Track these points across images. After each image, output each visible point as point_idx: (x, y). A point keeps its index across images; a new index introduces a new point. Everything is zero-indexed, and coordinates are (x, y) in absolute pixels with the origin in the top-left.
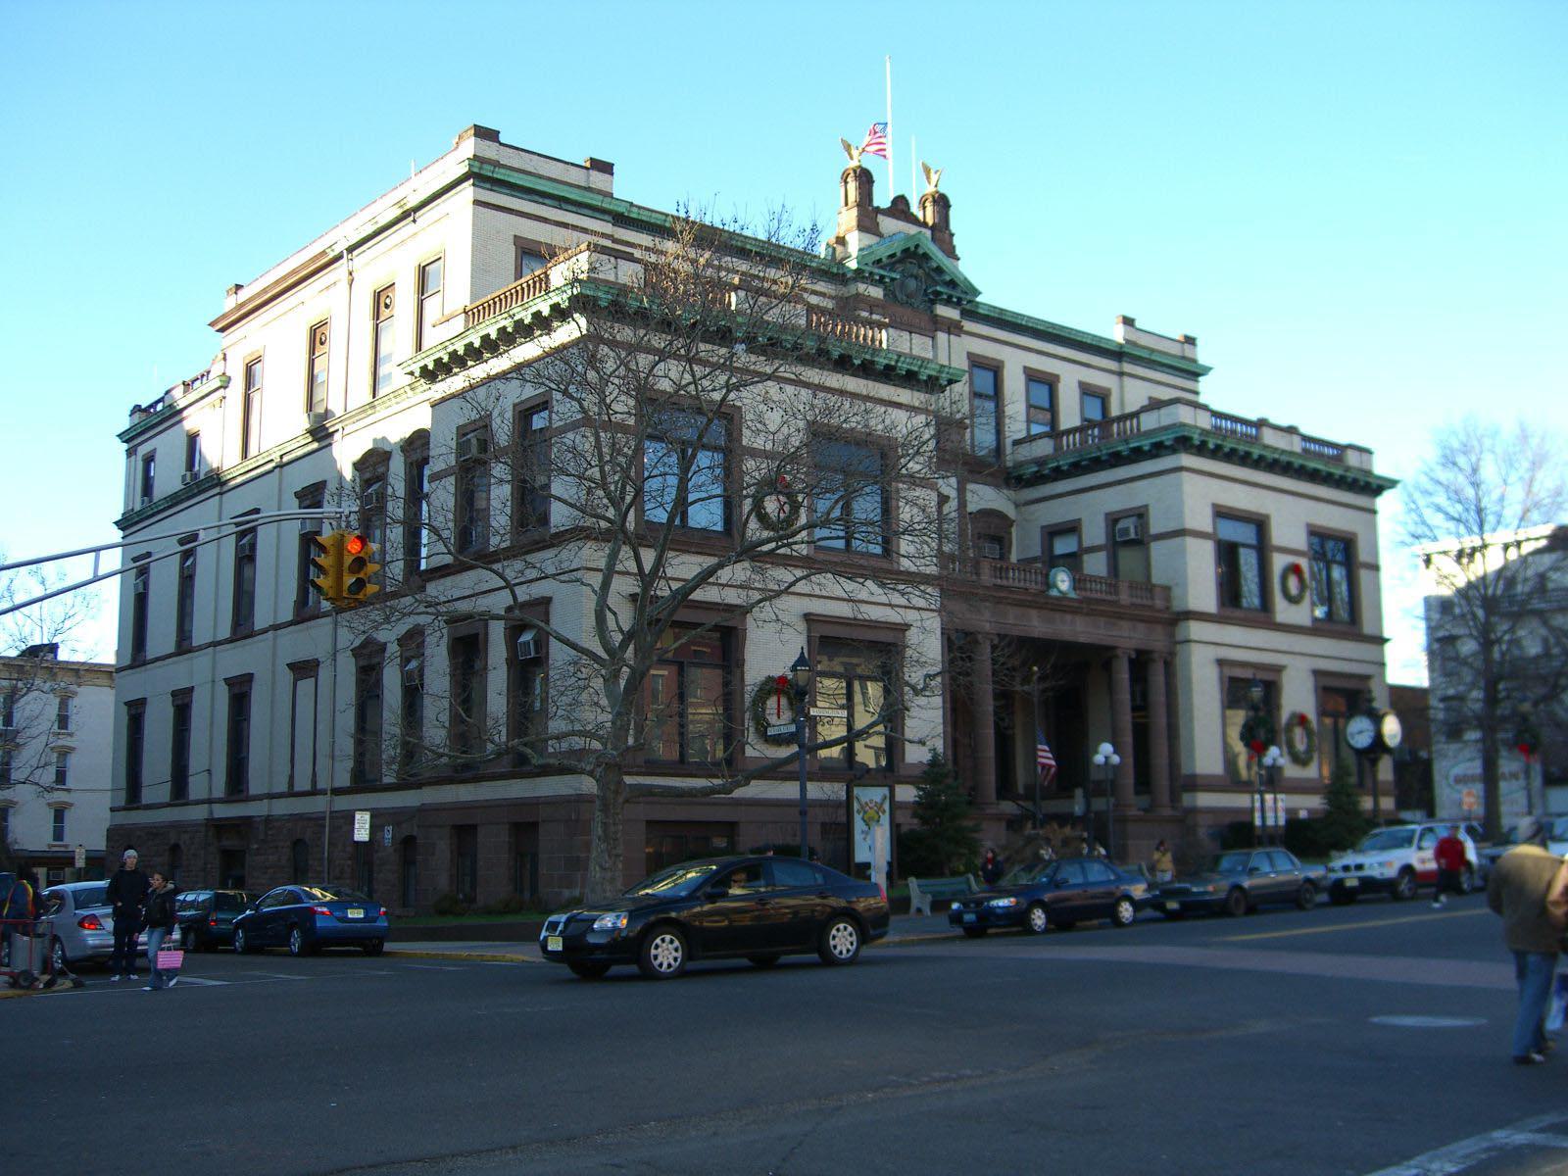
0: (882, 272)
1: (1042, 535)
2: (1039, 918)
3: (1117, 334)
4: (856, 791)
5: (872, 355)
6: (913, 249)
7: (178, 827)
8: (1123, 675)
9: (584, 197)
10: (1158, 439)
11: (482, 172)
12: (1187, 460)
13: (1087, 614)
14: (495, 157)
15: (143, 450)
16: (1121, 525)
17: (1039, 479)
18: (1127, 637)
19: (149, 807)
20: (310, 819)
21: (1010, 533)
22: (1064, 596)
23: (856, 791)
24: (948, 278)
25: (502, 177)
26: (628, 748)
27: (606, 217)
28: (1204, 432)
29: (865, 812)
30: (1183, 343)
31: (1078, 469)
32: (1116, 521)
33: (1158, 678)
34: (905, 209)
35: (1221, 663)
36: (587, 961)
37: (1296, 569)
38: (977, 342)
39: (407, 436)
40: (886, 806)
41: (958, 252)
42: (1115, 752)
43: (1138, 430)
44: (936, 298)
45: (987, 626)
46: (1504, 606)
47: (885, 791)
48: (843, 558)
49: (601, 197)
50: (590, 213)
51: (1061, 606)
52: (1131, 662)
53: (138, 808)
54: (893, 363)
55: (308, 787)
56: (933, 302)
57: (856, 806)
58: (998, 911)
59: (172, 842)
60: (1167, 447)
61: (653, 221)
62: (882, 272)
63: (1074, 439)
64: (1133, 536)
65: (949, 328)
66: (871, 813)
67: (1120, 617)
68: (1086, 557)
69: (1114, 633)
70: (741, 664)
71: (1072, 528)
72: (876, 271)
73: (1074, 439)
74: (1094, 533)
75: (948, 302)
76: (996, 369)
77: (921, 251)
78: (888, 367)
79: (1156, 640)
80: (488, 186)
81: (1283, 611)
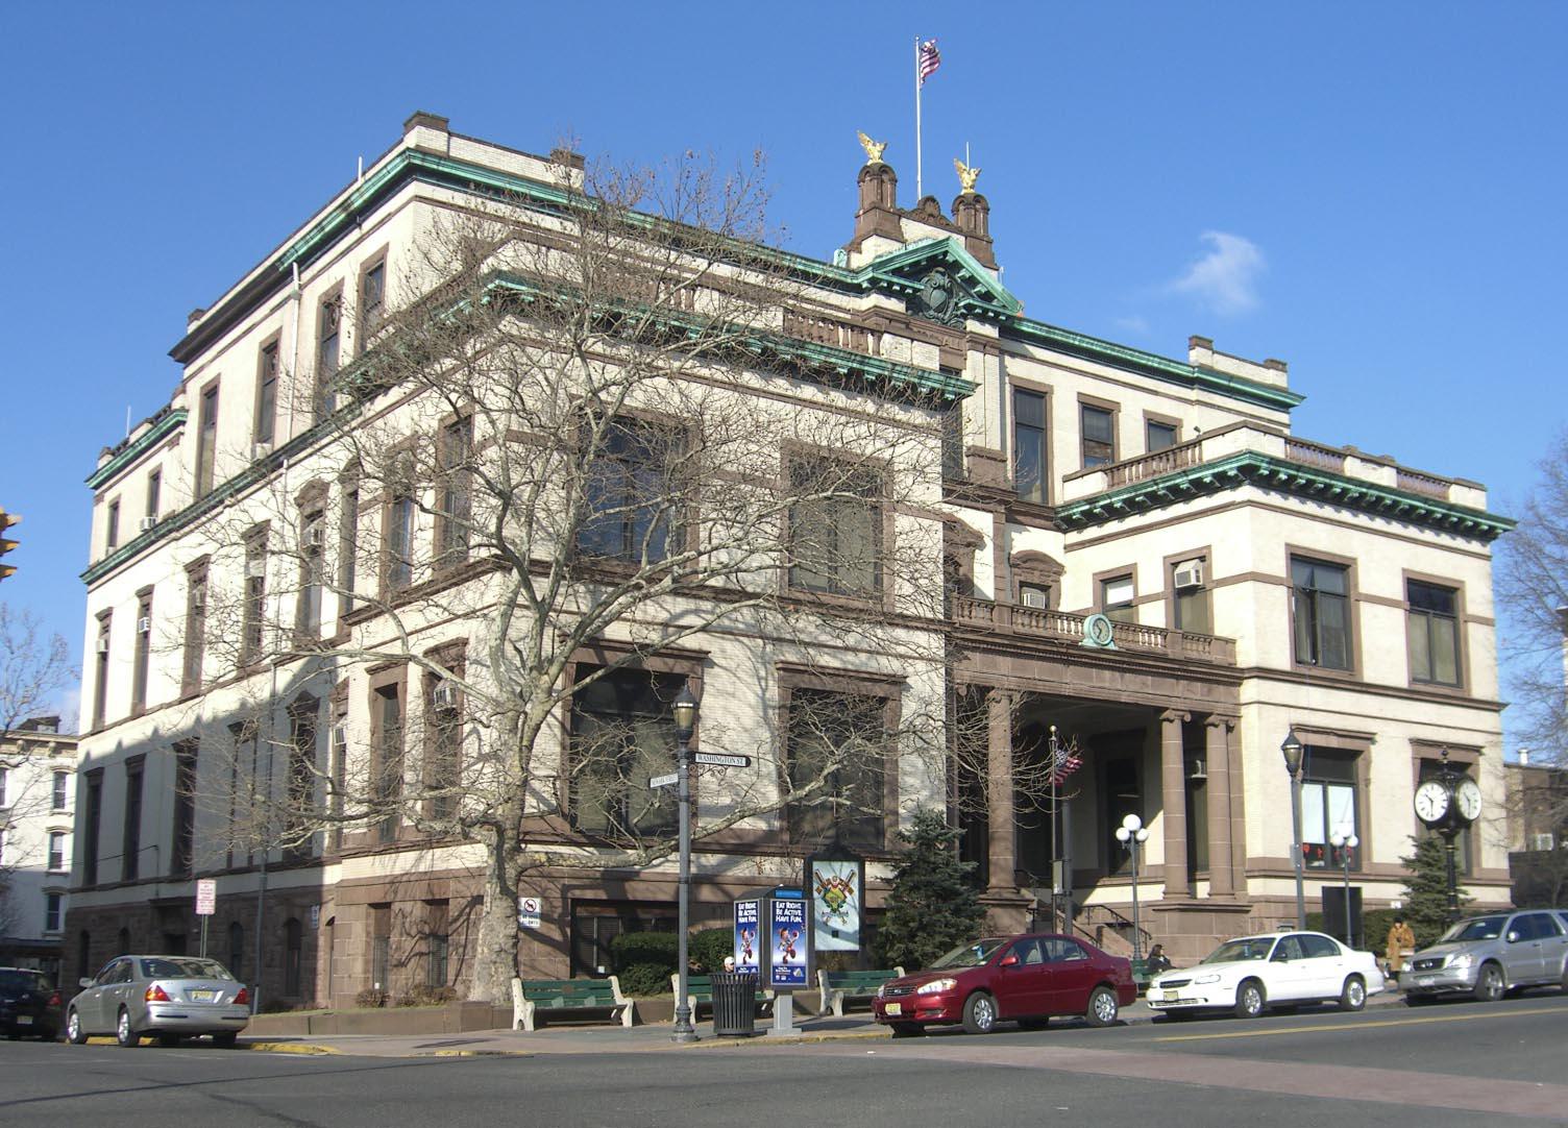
0: (902, 282)
1: (1094, 583)
7: (126, 908)
8: (1172, 739)
10: (1221, 469)
12: (1247, 492)
15: (109, 496)
16: (1181, 569)
17: (1090, 519)
18: (1181, 696)
19: (105, 888)
20: (245, 899)
23: (816, 865)
28: (1273, 461)
29: (827, 891)
31: (1134, 507)
32: (1175, 565)
33: (1215, 739)
35: (1417, 743)
39: (976, 581)
40: (855, 885)
43: (1200, 459)
46: (757, 483)
53: (93, 889)
55: (244, 864)
59: (122, 926)
62: (902, 282)
63: (1137, 471)
64: (1193, 582)
68: (1141, 608)
71: (1125, 576)
72: (895, 280)
73: (1137, 471)
74: (1152, 580)
75: (983, 318)
77: (950, 258)
78: (881, 379)
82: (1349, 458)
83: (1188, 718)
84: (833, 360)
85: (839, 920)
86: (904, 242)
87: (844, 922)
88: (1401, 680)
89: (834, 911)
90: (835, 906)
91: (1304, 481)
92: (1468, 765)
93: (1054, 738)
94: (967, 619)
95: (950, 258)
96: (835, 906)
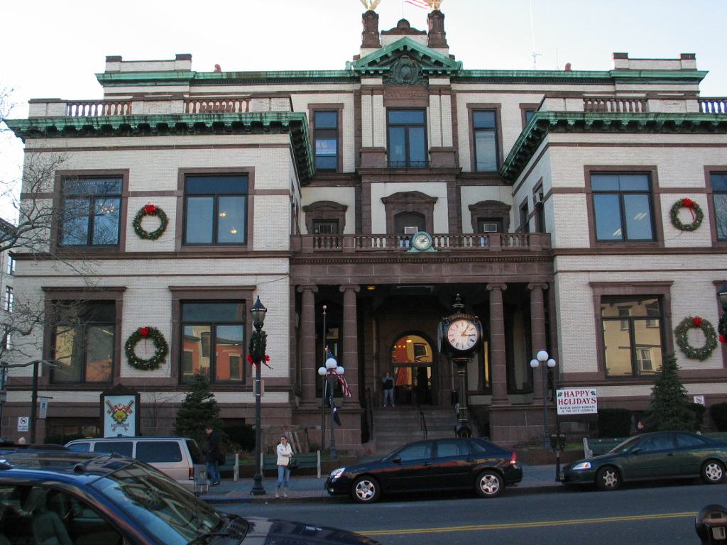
2: (610, 479)
3: (609, 65)
4: (106, 398)
5: (219, 116)
6: (402, 49)
9: (136, 76)
11: (113, 79)
13: (451, 262)
14: (118, 69)
21: (508, 214)
22: (422, 252)
23: (106, 398)
24: (433, 61)
25: (117, 78)
26: (399, 367)
27: (185, 83)
29: (114, 413)
30: (680, 60)
34: (407, 27)
35: (593, 285)
36: (572, 484)
37: (687, 204)
38: (470, 96)
40: (133, 408)
41: (448, 43)
42: (339, 364)
44: (426, 75)
45: (349, 280)
47: (133, 398)
48: (623, 246)
49: (176, 74)
50: (143, 84)
51: (422, 259)
52: (505, 294)
54: (238, 120)
56: (427, 78)
57: (107, 408)
58: (579, 472)
60: (39, 132)
61: (214, 78)
65: (440, 91)
66: (120, 413)
67: (490, 261)
69: (484, 273)
70: (669, 315)
75: (436, 75)
76: (494, 110)
77: (409, 49)
79: (533, 274)
80: (113, 85)
81: (672, 237)
82: (649, 101)
83: (505, 288)
84: (201, 121)
85: (123, 428)
86: (380, 47)
87: (126, 429)
88: (585, 243)
89: (119, 423)
90: (120, 420)
91: (591, 123)
92: (113, 302)
93: (324, 313)
94: (526, 246)
95: (409, 49)
96: (120, 420)
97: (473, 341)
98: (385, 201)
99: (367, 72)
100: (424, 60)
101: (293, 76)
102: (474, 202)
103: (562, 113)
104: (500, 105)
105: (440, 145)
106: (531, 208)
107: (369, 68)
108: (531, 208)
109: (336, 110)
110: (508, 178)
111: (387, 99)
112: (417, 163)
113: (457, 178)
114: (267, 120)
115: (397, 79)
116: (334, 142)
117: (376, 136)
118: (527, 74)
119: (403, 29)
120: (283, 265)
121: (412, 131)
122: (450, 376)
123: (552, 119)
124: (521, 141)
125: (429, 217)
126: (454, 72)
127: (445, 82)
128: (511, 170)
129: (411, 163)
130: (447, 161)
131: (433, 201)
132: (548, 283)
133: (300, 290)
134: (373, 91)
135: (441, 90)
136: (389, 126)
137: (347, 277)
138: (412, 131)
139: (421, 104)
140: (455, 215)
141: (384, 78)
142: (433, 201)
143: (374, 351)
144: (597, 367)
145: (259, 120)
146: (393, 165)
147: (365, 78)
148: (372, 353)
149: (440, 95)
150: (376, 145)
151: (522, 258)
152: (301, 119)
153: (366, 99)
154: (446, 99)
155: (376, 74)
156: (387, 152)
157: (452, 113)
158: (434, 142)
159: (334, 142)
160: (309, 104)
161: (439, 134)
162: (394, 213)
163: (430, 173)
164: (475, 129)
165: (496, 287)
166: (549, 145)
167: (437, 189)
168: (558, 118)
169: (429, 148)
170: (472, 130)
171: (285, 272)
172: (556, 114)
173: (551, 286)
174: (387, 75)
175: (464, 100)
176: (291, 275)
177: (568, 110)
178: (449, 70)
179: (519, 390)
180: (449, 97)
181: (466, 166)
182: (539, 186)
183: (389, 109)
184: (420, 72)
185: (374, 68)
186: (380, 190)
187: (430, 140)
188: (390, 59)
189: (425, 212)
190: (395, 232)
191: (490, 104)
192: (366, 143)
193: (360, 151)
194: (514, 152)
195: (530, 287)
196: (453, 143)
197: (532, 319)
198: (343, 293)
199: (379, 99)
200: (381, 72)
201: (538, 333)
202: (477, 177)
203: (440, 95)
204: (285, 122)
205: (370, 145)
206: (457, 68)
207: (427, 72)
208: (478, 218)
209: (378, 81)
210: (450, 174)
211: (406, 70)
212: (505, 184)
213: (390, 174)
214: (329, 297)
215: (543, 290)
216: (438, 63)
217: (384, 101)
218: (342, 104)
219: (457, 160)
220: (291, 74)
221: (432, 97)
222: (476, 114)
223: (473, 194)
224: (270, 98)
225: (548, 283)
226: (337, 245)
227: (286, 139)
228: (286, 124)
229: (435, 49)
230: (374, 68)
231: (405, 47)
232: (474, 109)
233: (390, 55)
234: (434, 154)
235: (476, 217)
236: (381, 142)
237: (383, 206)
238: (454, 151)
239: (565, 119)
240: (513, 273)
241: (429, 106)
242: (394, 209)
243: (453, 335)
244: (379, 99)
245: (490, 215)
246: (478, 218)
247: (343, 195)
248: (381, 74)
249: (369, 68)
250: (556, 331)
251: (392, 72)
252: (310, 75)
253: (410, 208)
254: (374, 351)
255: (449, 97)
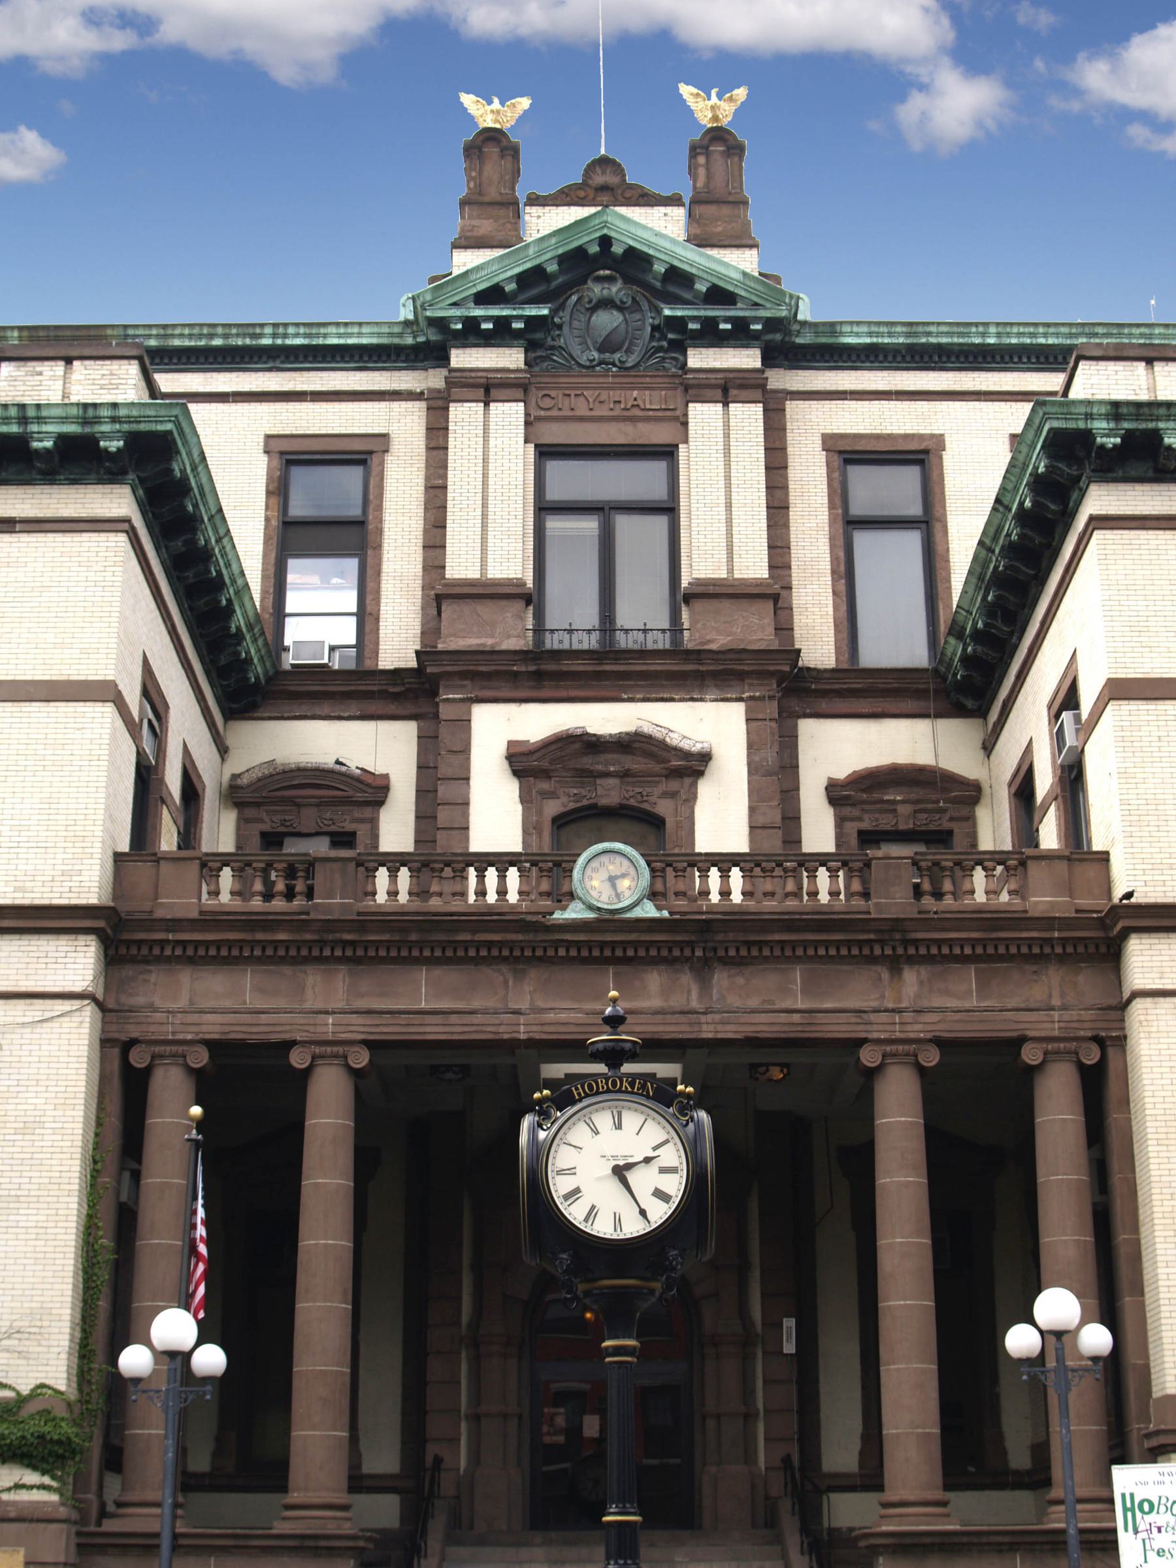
6: (594, 249)
24: (701, 287)
38: (837, 410)
44: (679, 337)
56: (680, 347)
75: (711, 336)
76: (921, 456)
77: (617, 249)
79: (1036, 1006)
95: (617, 249)
97: (560, 1172)
98: (524, 762)
99: (472, 324)
100: (672, 289)
101: (217, 342)
102: (841, 773)
103: (1140, 409)
104: (938, 442)
105: (723, 574)
106: (1044, 781)
107: (478, 312)
108: (1044, 781)
109: (363, 455)
110: (965, 687)
111: (539, 419)
112: (641, 635)
113: (787, 692)
114: (45, 428)
115: (576, 351)
116: (351, 565)
117: (493, 541)
118: (1033, 335)
119: (604, 188)
120: (76, 963)
121: (624, 524)
122: (749, 1417)
123: (1100, 425)
124: (999, 529)
125: (679, 826)
126: (772, 324)
127: (748, 359)
128: (974, 669)
129: (620, 636)
130: (751, 629)
131: (694, 765)
132: (1099, 1041)
133: (138, 1059)
134: (488, 388)
135: (727, 388)
136: (544, 508)
137: (322, 1010)
138: (624, 524)
139: (658, 434)
140: (775, 817)
141: (530, 347)
142: (694, 765)
143: (465, 1317)
144: (498, 576)
145: (14, 429)
146: (552, 642)
147: (465, 346)
148: (458, 1323)
149: (726, 404)
150: (496, 572)
151: (1003, 945)
152: (169, 426)
153: (464, 416)
154: (748, 417)
155: (501, 334)
156: (531, 598)
157: (769, 468)
158: (702, 562)
159: (352, 564)
160: (268, 437)
161: (721, 533)
162: (553, 808)
163: (687, 671)
164: (849, 524)
165: (894, 1055)
166: (1100, 522)
167: (713, 725)
168: (1126, 425)
169: (684, 583)
170: (840, 525)
171: (78, 988)
172: (1116, 410)
173: (1111, 1052)
174: (539, 336)
175: (810, 425)
176: (107, 1004)
177: (1159, 398)
178: (757, 320)
179: (1017, 1473)
180: (758, 409)
181: (818, 646)
182: (1068, 698)
183: (545, 453)
184: (655, 328)
185: (495, 311)
186: (497, 728)
187: (690, 557)
188: (554, 284)
189: (664, 808)
190: (548, 862)
191: (906, 437)
192: (461, 565)
193: (442, 596)
194: (981, 578)
195: (1030, 1055)
196: (771, 567)
197: (1041, 1180)
198: (305, 1074)
199: (509, 415)
200: (518, 325)
201: (1062, 1229)
202: (860, 690)
203: (726, 404)
204: (108, 436)
205: (473, 573)
206: (783, 312)
207: (678, 324)
208: (861, 833)
209: (511, 358)
210: (762, 675)
211: (607, 321)
212: (958, 711)
213: (540, 673)
214: (250, 1093)
215: (1082, 1068)
216: (719, 295)
217: (527, 423)
218: (385, 437)
219: (784, 628)
220: (211, 336)
221: (697, 412)
222: (856, 473)
223: (840, 748)
224: (69, 361)
225: (1099, 1041)
226: (290, 894)
227: (118, 501)
228: (114, 445)
229: (714, 252)
230: (495, 311)
231: (606, 242)
232: (848, 455)
233: (552, 268)
234: (698, 605)
235: (852, 828)
236: (510, 562)
237: (512, 788)
238: (773, 595)
239: (1151, 425)
240: (958, 1003)
241: (686, 441)
242: (552, 795)
243: (571, 1171)
244: (509, 415)
245: (906, 815)
246: (861, 833)
247: (381, 747)
248: (518, 334)
249: (478, 312)
250: (1135, 1227)
251: (560, 327)
252: (274, 336)
253: (610, 793)
254: (465, 1317)
255: (758, 409)
